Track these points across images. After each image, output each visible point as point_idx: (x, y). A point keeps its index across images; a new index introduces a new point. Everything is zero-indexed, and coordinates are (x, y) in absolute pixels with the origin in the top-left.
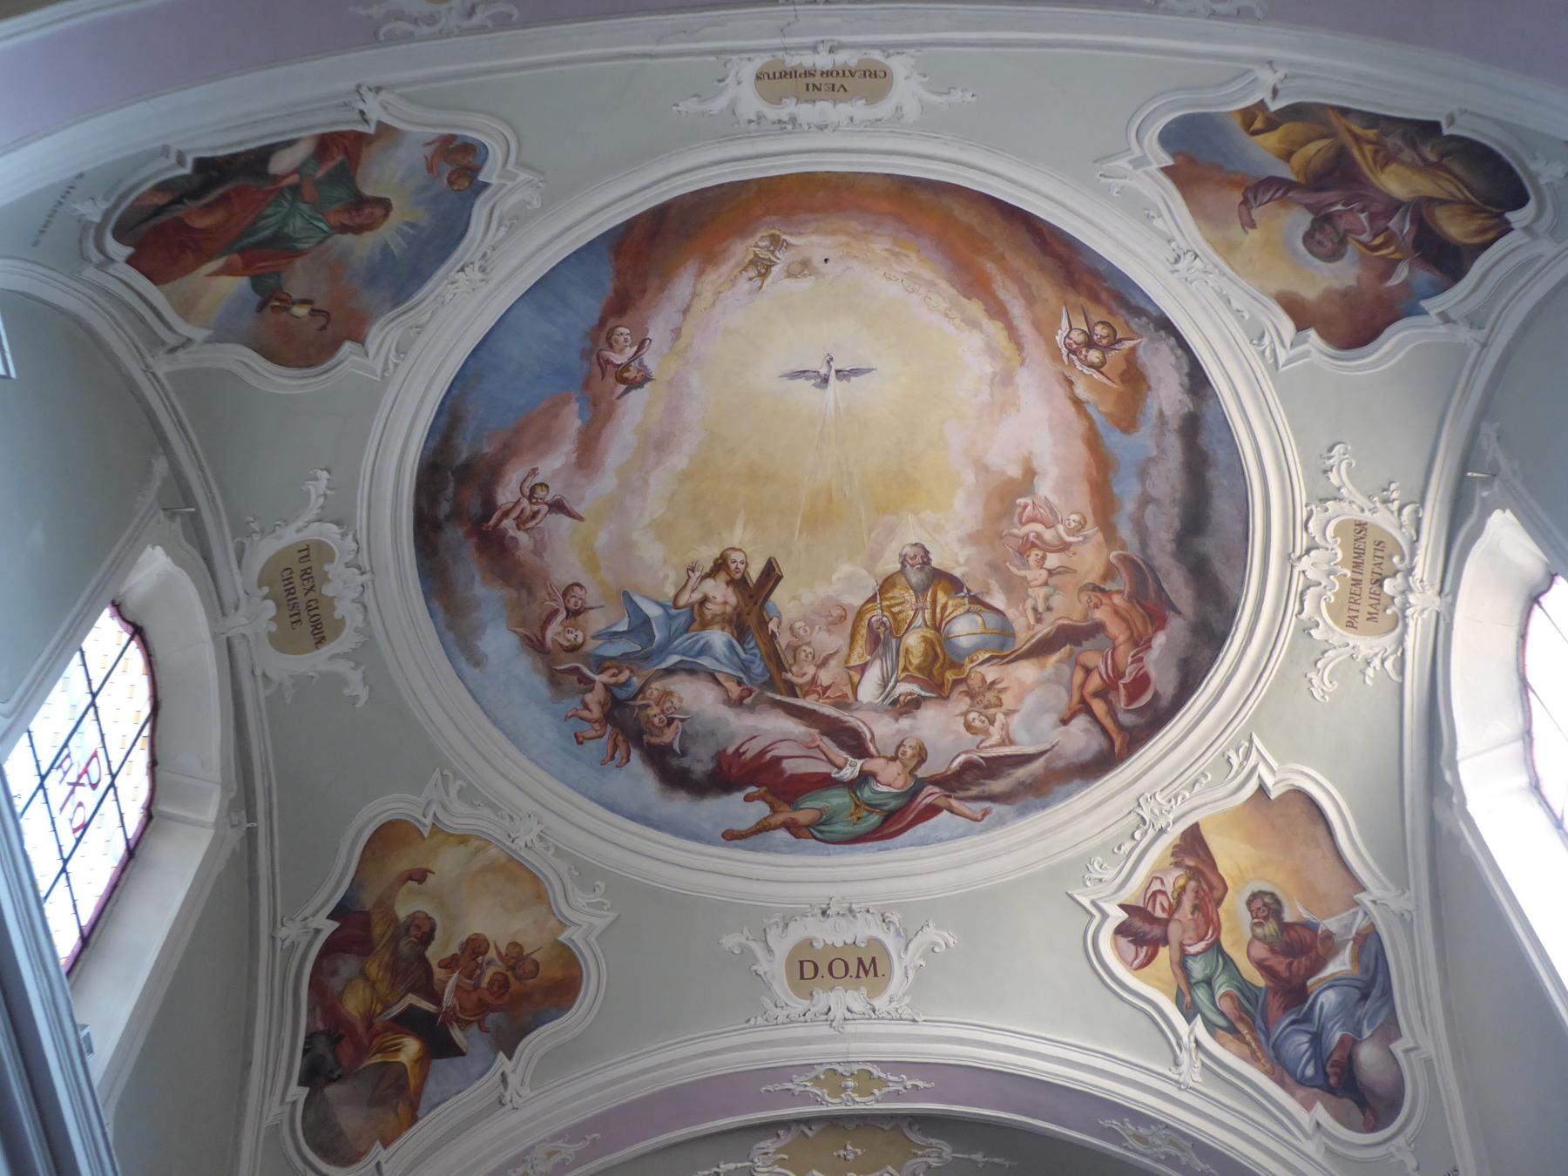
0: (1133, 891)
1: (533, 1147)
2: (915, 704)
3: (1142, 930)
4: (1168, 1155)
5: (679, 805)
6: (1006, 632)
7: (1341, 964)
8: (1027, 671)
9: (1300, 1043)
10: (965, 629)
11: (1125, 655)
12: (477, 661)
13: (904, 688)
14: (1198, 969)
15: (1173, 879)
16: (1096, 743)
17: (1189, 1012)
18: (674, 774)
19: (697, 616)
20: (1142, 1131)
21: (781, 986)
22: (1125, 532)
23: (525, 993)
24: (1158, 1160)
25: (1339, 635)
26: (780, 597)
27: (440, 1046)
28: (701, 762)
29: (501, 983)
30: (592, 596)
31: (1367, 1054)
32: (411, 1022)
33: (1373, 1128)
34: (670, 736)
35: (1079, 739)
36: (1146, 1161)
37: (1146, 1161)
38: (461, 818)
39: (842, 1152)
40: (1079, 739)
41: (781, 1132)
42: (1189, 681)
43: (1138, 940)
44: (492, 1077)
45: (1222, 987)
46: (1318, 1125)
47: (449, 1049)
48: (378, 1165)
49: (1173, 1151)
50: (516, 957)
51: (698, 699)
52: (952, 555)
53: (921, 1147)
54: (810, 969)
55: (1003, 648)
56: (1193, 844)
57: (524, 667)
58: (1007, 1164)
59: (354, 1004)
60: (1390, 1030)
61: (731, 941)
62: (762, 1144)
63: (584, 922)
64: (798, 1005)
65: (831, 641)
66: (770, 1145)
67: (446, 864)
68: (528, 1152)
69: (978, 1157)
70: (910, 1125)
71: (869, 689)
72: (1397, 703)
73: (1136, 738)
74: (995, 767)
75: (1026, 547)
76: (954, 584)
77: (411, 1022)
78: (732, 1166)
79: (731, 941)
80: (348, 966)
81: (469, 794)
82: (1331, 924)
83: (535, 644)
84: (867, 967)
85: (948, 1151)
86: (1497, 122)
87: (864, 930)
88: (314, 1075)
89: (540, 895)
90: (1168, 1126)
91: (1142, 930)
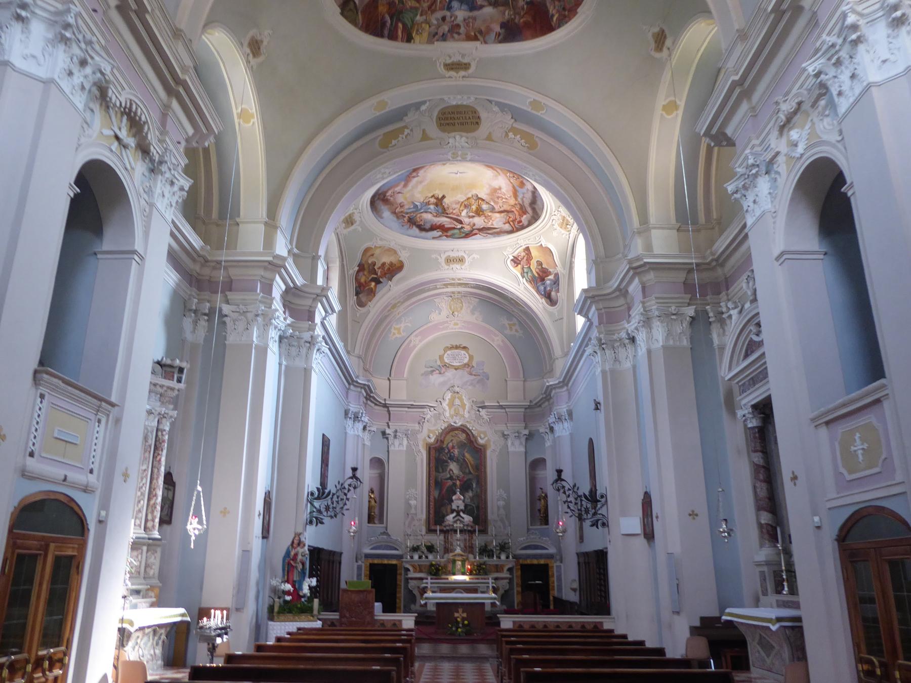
0: (515, 254)
2: (473, 217)
3: (516, 261)
5: (424, 234)
6: (493, 208)
7: (551, 277)
8: (498, 215)
9: (542, 288)
10: (485, 207)
11: (518, 217)
12: (382, 218)
13: (471, 214)
14: (525, 270)
15: (523, 254)
16: (510, 228)
17: (523, 277)
18: (422, 228)
19: (428, 203)
21: (443, 264)
22: (519, 200)
23: (393, 270)
25: (559, 228)
26: (445, 200)
27: (378, 282)
28: (428, 226)
29: (389, 269)
30: (405, 203)
31: (553, 294)
32: (373, 280)
34: (422, 223)
35: (507, 227)
38: (380, 243)
40: (507, 227)
42: (529, 224)
43: (515, 262)
44: (388, 286)
45: (530, 274)
47: (380, 282)
50: (391, 264)
51: (428, 217)
52: (482, 195)
54: (449, 261)
55: (493, 210)
56: (527, 249)
57: (393, 218)
59: (363, 280)
60: (558, 291)
61: (433, 256)
63: (404, 256)
64: (447, 267)
65: (454, 206)
67: (377, 252)
71: (464, 213)
73: (518, 230)
74: (489, 229)
75: (498, 198)
76: (483, 200)
77: (373, 280)
79: (433, 256)
80: (361, 274)
81: (381, 239)
82: (551, 270)
83: (394, 213)
84: (461, 260)
87: (461, 254)
88: (357, 294)
89: (395, 252)
91: (516, 261)
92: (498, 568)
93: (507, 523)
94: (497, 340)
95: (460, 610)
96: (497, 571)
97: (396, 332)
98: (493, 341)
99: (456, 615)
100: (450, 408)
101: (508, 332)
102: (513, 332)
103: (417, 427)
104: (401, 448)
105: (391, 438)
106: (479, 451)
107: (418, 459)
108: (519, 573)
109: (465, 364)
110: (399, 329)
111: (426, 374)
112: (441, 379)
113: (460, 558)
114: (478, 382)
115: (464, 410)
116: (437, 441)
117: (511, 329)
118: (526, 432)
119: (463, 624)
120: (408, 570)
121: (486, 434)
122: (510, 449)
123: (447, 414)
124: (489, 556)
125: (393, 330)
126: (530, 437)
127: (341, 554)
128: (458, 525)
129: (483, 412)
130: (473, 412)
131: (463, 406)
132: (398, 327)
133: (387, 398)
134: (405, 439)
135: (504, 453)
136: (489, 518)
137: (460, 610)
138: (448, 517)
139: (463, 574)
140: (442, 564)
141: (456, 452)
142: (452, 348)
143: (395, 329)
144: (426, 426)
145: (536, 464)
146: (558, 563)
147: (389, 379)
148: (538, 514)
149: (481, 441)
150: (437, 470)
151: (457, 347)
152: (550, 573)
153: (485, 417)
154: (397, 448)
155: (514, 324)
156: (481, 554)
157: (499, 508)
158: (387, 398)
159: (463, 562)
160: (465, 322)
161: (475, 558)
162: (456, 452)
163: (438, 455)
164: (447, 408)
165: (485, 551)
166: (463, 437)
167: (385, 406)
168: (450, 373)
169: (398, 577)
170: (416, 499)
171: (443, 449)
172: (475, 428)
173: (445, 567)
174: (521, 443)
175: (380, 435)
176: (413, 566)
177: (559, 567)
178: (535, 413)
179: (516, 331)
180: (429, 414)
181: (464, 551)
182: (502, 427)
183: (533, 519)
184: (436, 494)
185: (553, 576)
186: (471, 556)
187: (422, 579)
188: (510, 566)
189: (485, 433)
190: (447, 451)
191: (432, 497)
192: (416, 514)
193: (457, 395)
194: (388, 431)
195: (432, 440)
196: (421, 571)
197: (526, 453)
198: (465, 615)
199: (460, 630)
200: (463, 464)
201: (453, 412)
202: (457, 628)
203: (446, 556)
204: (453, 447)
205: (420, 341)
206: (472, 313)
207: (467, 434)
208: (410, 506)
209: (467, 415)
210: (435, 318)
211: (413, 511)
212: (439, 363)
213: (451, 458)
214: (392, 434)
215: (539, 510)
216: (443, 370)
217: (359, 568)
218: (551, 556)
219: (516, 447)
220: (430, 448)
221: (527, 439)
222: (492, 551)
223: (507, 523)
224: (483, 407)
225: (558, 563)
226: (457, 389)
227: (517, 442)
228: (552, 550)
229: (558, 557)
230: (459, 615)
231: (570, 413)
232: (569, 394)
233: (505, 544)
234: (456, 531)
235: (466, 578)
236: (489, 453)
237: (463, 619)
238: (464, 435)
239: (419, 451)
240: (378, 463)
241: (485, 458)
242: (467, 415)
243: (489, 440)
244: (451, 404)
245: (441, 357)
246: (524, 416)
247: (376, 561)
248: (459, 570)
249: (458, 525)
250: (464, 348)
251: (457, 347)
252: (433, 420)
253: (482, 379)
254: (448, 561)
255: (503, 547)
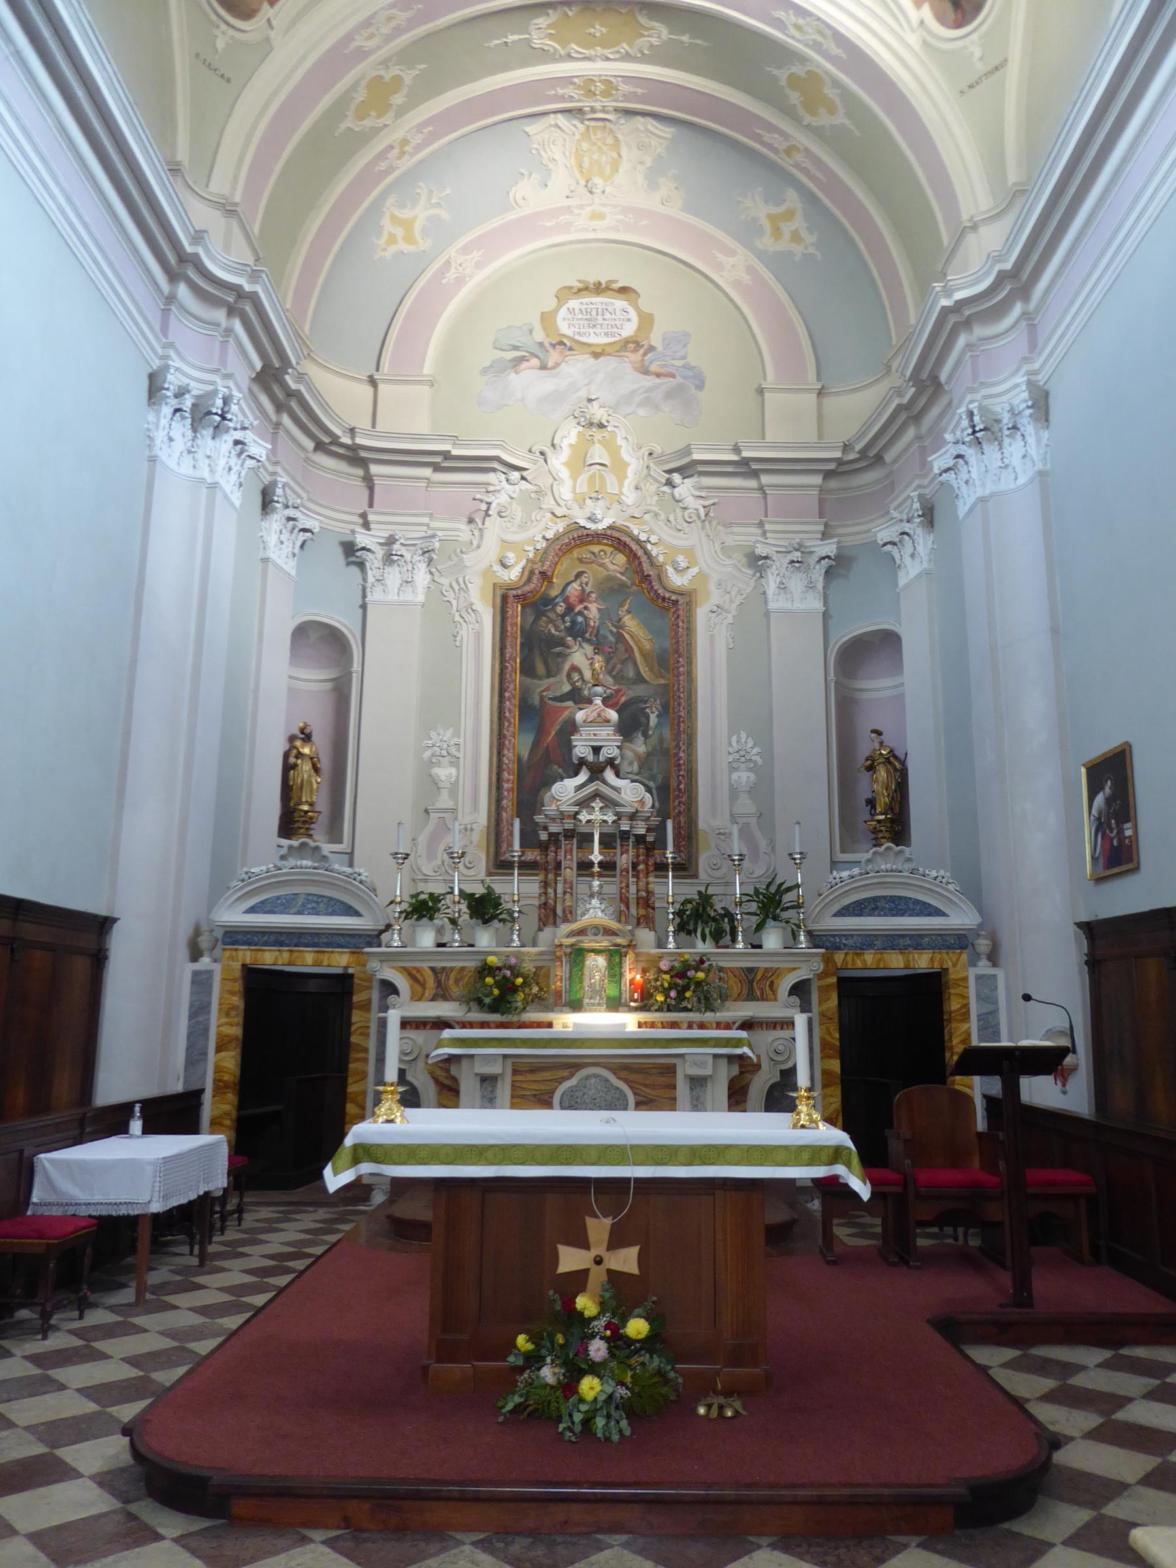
1: (376, 13)
4: (815, 41)
20: (801, 21)
24: (807, 45)
33: (958, 25)
36: (797, 45)
37: (797, 45)
39: (592, 30)
41: (550, 11)
46: (922, 22)
48: (269, 20)
49: (819, 39)
53: (647, 29)
58: (706, 44)
62: (536, 21)
66: (542, 21)
68: (372, 16)
69: (685, 38)
70: (641, 10)
72: (514, 122)
78: (516, 37)
85: (664, 32)
86: (296, 1220)
90: (819, 19)
92: (755, 984)
93: (763, 844)
94: (733, 267)
95: (599, 1227)
96: (751, 997)
97: (399, 232)
98: (719, 267)
99: (570, 1259)
100: (574, 477)
101: (766, 242)
102: (784, 245)
103: (464, 532)
104: (408, 596)
105: (374, 561)
106: (671, 609)
107: (464, 632)
108: (834, 1001)
109: (627, 342)
110: (408, 225)
111: (497, 369)
112: (546, 384)
113: (604, 943)
114: (669, 395)
115: (621, 478)
116: (529, 574)
117: (777, 232)
118: (829, 548)
119: (617, 1340)
120: (395, 991)
121: (694, 553)
122: (772, 605)
123: (565, 492)
124: (717, 936)
125: (386, 222)
126: (837, 567)
127: (102, 925)
128: (596, 817)
129: (685, 488)
130: (652, 488)
131: (620, 468)
132: (405, 214)
133: (364, 423)
134: (422, 567)
135: (754, 617)
136: (702, 824)
137: (599, 1227)
138: (557, 788)
139: (615, 1005)
140: (528, 967)
141: (593, 611)
142: (584, 289)
143: (395, 220)
144: (494, 528)
145: (863, 654)
146: (984, 967)
147: (373, 382)
148: (864, 813)
149: (677, 580)
150: (528, 669)
151: (599, 289)
152: (954, 1005)
153: (691, 502)
154: (392, 597)
155: (789, 215)
156: (684, 928)
157: (734, 793)
158: (364, 423)
159: (616, 956)
160: (625, 210)
161: (661, 944)
162: (593, 611)
163: (534, 623)
164: (564, 473)
165: (697, 917)
166: (616, 563)
167: (355, 457)
168: (576, 368)
169: (356, 1016)
170: (455, 762)
171: (548, 601)
172: (660, 537)
173: (540, 976)
174: (811, 586)
175: (339, 552)
176: (413, 976)
177: (987, 981)
178: (860, 480)
179: (796, 237)
180: (503, 490)
181: (620, 917)
182: (746, 536)
183: (848, 832)
184: (521, 744)
185: (966, 1016)
186: (646, 936)
187: (441, 1024)
188: (802, 974)
189: (689, 552)
190: (560, 609)
191: (509, 754)
192: (454, 811)
193: (598, 434)
194: (362, 539)
195: (513, 575)
196: (441, 995)
197: (826, 616)
198: (627, 1260)
199: (590, 1387)
200: (613, 648)
201: (583, 486)
202: (576, 1369)
203: (546, 934)
204: (583, 597)
205: (479, 265)
206: (653, 177)
207: (632, 556)
208: (434, 782)
209: (630, 497)
210: (529, 197)
211: (444, 801)
212: (539, 335)
213: (577, 632)
214: (380, 552)
215: (871, 803)
216: (554, 356)
217: (201, 982)
218: (960, 941)
219: (795, 598)
220: (505, 599)
221: (828, 573)
222: (731, 917)
223: (763, 844)
224: (686, 470)
225: (984, 967)
226: (598, 413)
227: (797, 583)
228: (961, 918)
229: (983, 945)
230: (592, 1257)
231: (1041, 404)
232: (1032, 329)
233: (782, 891)
234: (585, 840)
235: (629, 1022)
236: (701, 615)
237: (623, 1294)
238: (621, 559)
239: (471, 608)
240: (324, 643)
241: (690, 630)
242: (630, 497)
243: (702, 576)
244: (579, 461)
245: (548, 319)
246: (821, 501)
247: (270, 958)
248: (595, 993)
249: (596, 817)
250: (624, 290)
251: (599, 289)
252: (517, 510)
253: (683, 386)
254: (555, 953)
255: (771, 903)
